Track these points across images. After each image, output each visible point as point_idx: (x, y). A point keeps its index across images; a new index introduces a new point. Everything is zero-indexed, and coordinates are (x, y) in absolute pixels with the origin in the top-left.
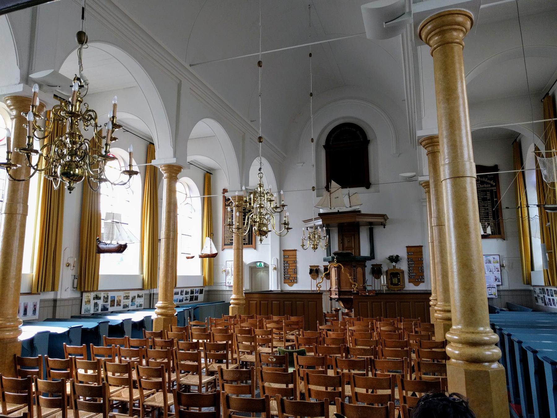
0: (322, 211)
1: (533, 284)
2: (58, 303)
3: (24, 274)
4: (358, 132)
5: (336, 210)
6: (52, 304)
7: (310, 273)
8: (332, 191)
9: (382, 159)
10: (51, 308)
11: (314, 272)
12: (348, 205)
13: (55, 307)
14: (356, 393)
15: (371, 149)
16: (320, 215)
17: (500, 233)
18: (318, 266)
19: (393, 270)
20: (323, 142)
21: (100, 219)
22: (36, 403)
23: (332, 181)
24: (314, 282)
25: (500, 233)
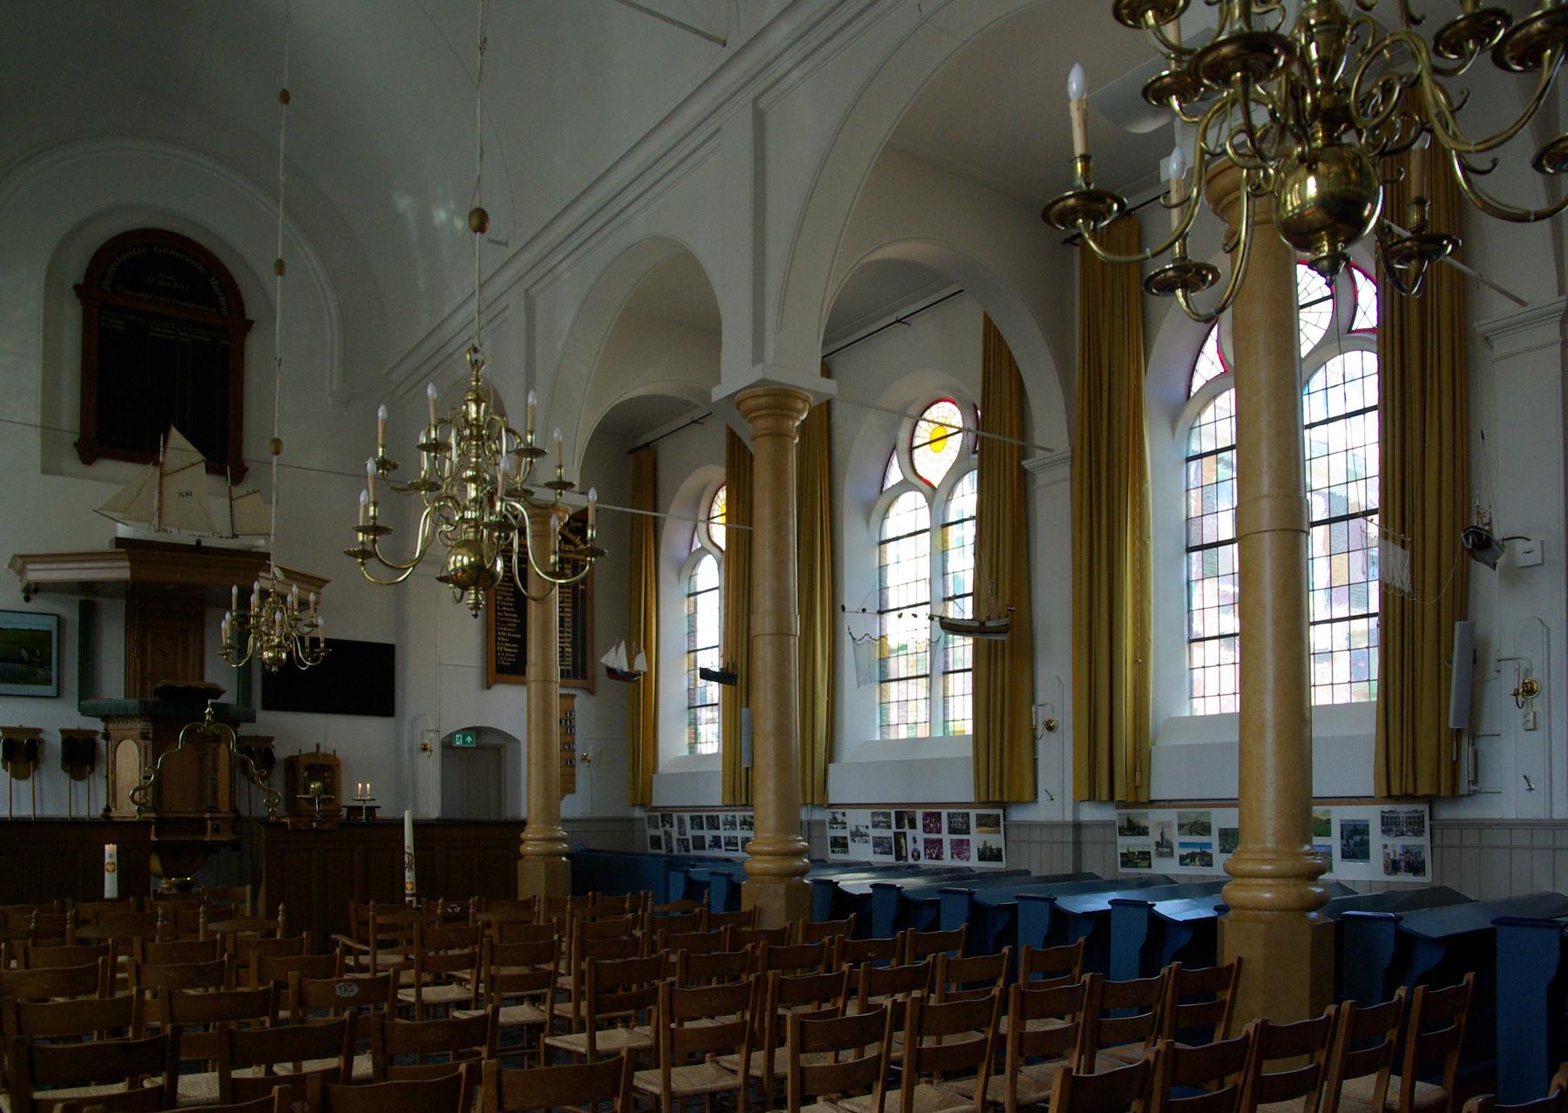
0: (123, 531)
1: (833, 798)
2: (1087, 835)
3: (674, 777)
4: (213, 281)
5: (186, 537)
6: (1069, 836)
7: (8, 756)
8: (169, 467)
9: (286, 387)
10: (1069, 849)
12: (227, 532)
13: (1077, 844)
14: (802, 1069)
15: (254, 347)
16: (120, 542)
17: (584, 677)
18: (39, 731)
19: (316, 755)
20: (75, 271)
21: (975, 670)
22: (904, 1085)
23: (174, 432)
25: (584, 677)
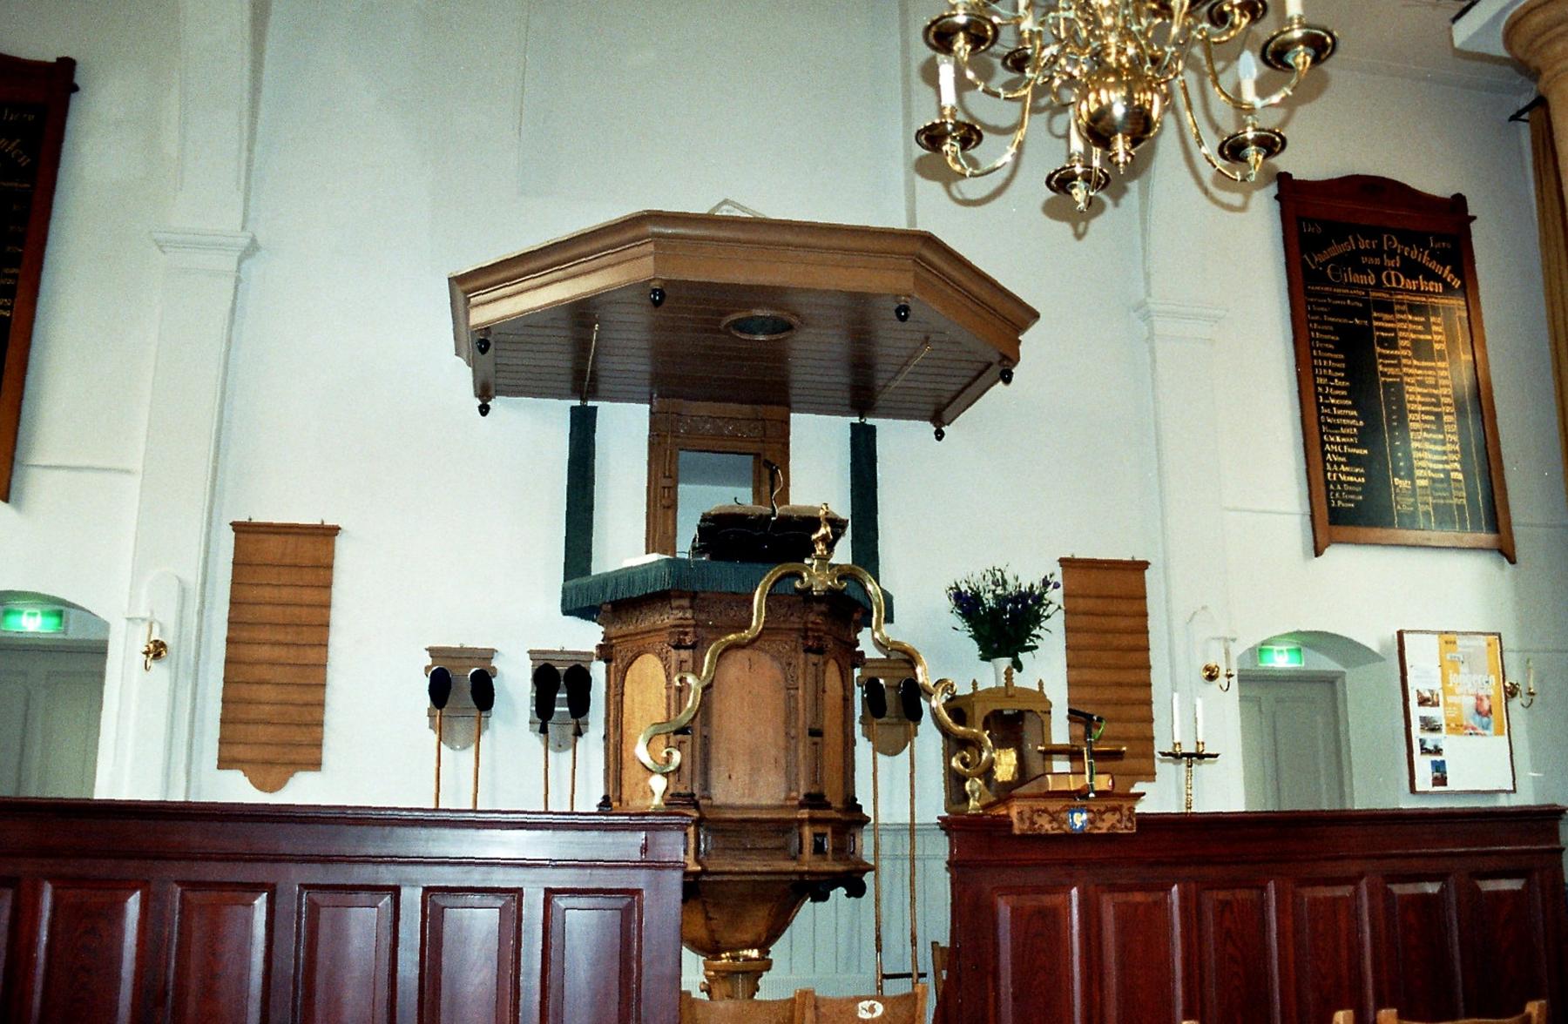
11: (460, 688)
24: (458, 761)
